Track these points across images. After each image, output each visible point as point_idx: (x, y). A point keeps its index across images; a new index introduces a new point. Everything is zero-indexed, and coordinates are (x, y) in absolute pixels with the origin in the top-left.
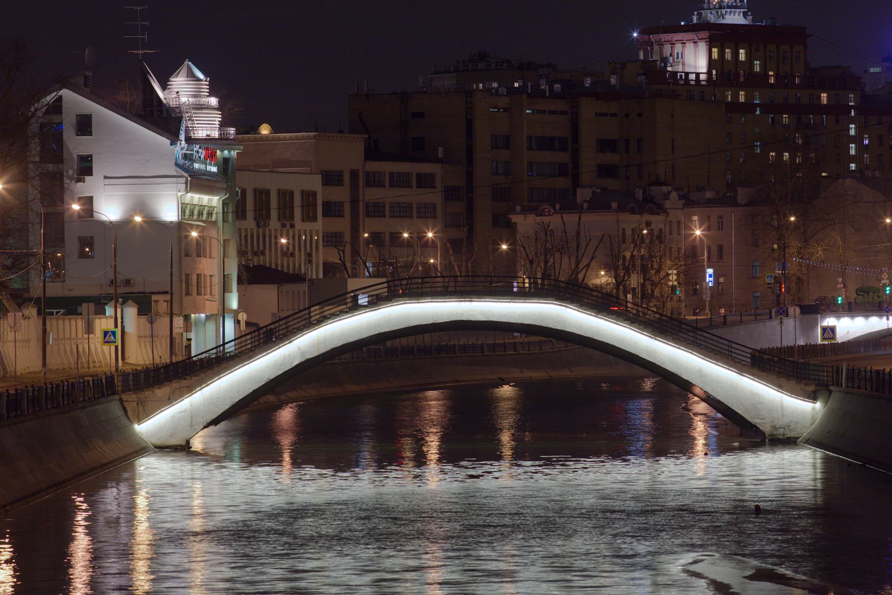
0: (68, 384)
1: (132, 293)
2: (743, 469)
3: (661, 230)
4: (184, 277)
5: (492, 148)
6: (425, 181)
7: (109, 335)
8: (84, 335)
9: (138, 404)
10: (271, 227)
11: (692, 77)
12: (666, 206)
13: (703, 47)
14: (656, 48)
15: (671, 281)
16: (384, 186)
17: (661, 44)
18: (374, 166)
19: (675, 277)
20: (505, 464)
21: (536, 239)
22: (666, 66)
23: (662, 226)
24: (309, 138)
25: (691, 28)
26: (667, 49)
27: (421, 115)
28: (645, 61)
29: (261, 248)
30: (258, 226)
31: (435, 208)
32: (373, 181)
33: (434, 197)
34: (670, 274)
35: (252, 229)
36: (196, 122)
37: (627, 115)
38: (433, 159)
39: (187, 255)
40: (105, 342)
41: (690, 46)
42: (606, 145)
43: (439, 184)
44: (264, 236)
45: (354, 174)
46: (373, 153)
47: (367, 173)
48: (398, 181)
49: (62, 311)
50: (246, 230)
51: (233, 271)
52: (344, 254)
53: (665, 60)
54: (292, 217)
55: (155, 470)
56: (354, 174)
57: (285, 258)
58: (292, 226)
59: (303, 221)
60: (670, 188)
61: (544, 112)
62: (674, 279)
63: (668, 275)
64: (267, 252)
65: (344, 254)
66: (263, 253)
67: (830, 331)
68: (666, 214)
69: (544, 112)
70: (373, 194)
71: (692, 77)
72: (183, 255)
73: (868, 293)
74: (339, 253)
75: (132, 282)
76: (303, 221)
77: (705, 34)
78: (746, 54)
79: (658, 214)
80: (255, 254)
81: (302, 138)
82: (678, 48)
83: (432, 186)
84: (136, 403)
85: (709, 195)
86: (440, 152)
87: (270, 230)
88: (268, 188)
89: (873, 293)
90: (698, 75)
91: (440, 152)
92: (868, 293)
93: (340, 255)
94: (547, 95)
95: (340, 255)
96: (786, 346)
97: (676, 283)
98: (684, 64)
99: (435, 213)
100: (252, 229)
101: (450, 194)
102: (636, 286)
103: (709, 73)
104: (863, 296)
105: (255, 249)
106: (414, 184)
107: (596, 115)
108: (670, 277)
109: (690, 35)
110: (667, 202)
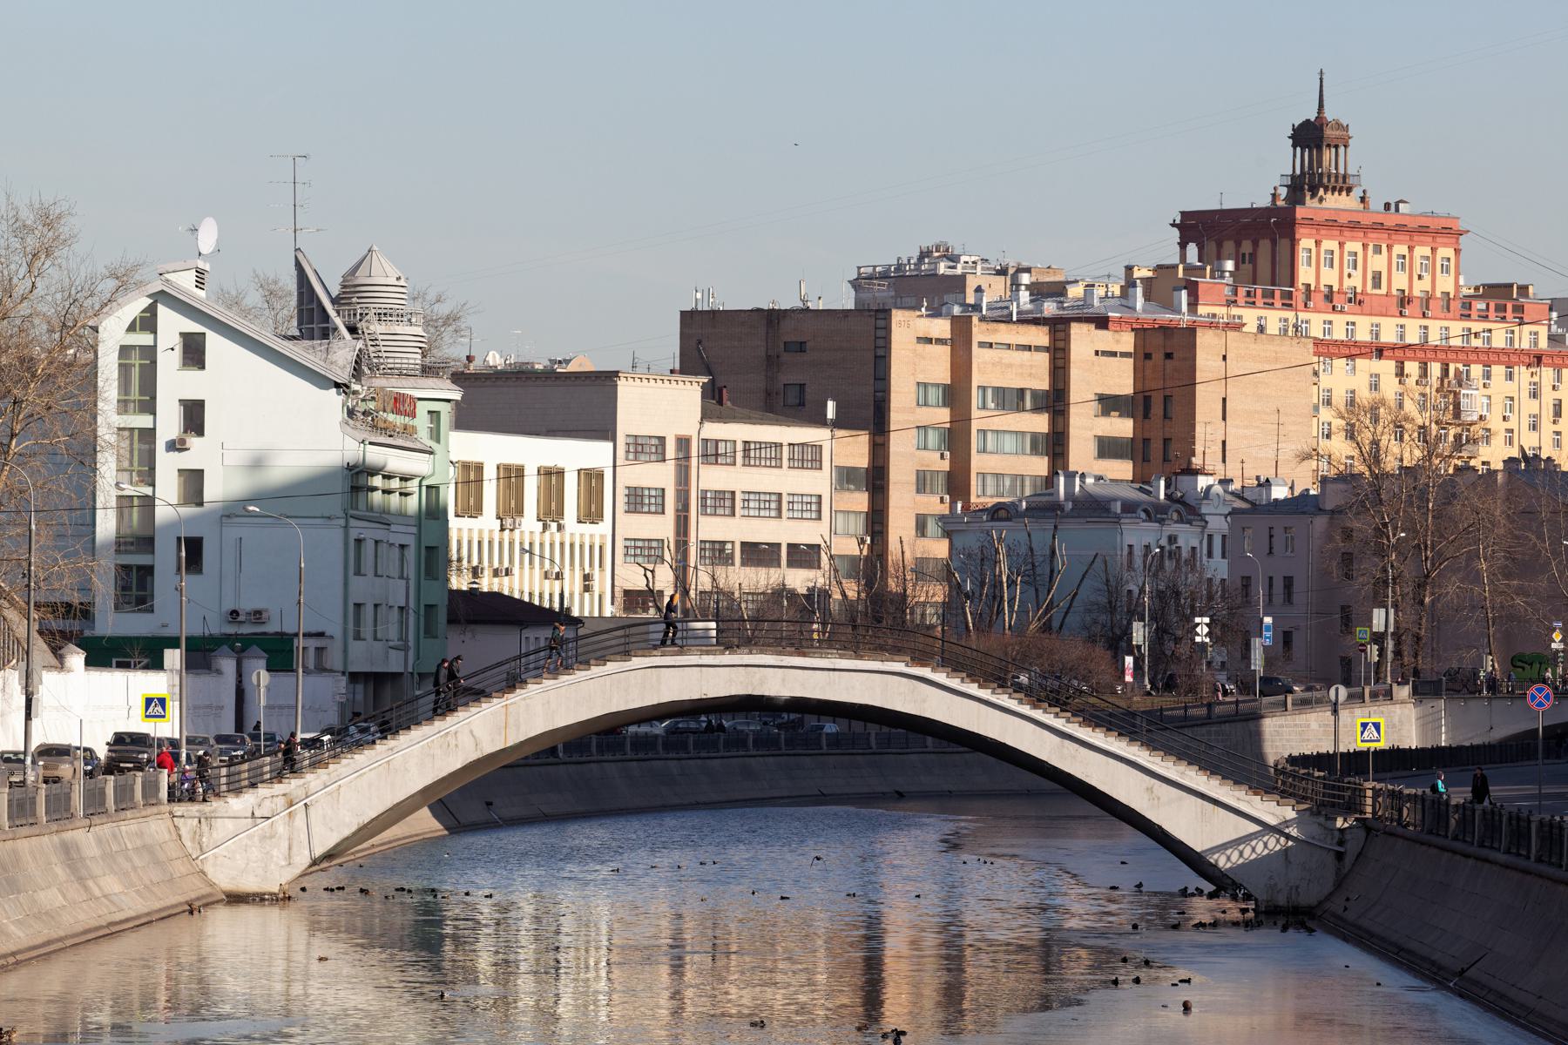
1: (265, 634)
3: (1194, 549)
5: (918, 404)
6: (808, 457)
7: (153, 704)
9: (200, 822)
10: (523, 527)
15: (1198, 635)
18: (715, 430)
19: (1206, 630)
21: (982, 560)
23: (1195, 543)
27: (801, 347)
29: (506, 564)
32: (713, 453)
34: (1198, 624)
35: (491, 531)
36: (383, 349)
40: (147, 716)
45: (683, 443)
49: (145, 661)
50: (481, 532)
52: (653, 577)
54: (560, 512)
55: (895, 945)
56: (683, 443)
58: (560, 528)
62: (1204, 633)
64: (516, 570)
65: (653, 577)
66: (508, 572)
67: (1373, 729)
68: (1203, 524)
69: (1029, 348)
70: (711, 478)
73: (1531, 664)
74: (645, 575)
75: (264, 615)
80: (496, 573)
83: (817, 463)
84: (196, 820)
89: (1540, 664)
92: (1531, 664)
93: (647, 578)
94: (1015, 319)
95: (647, 578)
96: (1352, 751)
97: (1207, 640)
100: (491, 531)
101: (846, 477)
102: (1141, 643)
104: (1523, 669)
106: (490, 473)
108: (1198, 630)
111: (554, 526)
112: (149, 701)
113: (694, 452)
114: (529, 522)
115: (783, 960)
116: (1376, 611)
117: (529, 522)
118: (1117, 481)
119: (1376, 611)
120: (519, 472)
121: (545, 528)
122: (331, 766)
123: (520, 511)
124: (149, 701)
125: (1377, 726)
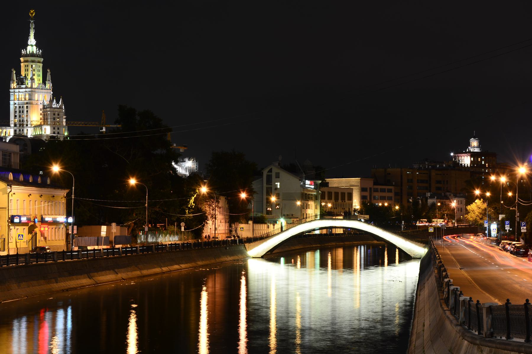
0: (228, 244)
2: (39, 346)
4: (302, 214)
6: (390, 191)
8: (487, 226)
11: (466, 165)
12: (450, 198)
13: (469, 157)
14: (457, 157)
16: (378, 192)
17: (458, 157)
18: (376, 187)
20: (386, 267)
22: (459, 162)
24: (359, 179)
25: (466, 153)
26: (460, 158)
27: (390, 174)
28: (454, 161)
30: (335, 201)
31: (392, 198)
32: (376, 190)
33: (391, 195)
37: (444, 174)
38: (392, 185)
39: (303, 209)
41: (466, 157)
42: (439, 182)
43: (393, 191)
44: (337, 204)
45: (370, 189)
46: (375, 184)
47: (374, 188)
48: (383, 191)
51: (319, 213)
53: (459, 161)
54: (345, 199)
56: (370, 189)
57: (343, 210)
58: (345, 202)
59: (348, 200)
60: (451, 193)
61: (422, 173)
63: (495, 216)
64: (338, 208)
66: (336, 208)
67: (21, 236)
69: (422, 173)
71: (466, 165)
72: (302, 208)
76: (348, 200)
77: (469, 154)
78: (480, 159)
79: (447, 200)
81: (357, 179)
82: (463, 158)
85: (462, 195)
86: (394, 183)
87: (339, 203)
88: (345, 192)
90: (467, 164)
91: (394, 183)
98: (464, 162)
99: (392, 199)
101: (396, 194)
103: (471, 164)
105: (343, 207)
107: (436, 174)
109: (466, 154)
110: (450, 197)
111: (344, 201)
112: (19, 235)
113: (372, 190)
114: (340, 201)
115: (4, 175)
116: (109, 246)
117: (340, 201)
118: (41, 235)
119: (109, 246)
120: (338, 193)
121: (342, 201)
122: (46, 236)
123: (338, 199)
124: (19, 235)
125: (22, 235)
